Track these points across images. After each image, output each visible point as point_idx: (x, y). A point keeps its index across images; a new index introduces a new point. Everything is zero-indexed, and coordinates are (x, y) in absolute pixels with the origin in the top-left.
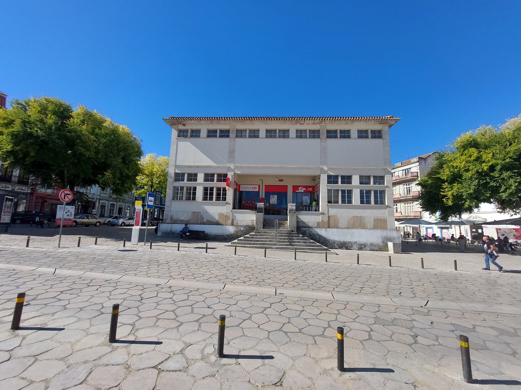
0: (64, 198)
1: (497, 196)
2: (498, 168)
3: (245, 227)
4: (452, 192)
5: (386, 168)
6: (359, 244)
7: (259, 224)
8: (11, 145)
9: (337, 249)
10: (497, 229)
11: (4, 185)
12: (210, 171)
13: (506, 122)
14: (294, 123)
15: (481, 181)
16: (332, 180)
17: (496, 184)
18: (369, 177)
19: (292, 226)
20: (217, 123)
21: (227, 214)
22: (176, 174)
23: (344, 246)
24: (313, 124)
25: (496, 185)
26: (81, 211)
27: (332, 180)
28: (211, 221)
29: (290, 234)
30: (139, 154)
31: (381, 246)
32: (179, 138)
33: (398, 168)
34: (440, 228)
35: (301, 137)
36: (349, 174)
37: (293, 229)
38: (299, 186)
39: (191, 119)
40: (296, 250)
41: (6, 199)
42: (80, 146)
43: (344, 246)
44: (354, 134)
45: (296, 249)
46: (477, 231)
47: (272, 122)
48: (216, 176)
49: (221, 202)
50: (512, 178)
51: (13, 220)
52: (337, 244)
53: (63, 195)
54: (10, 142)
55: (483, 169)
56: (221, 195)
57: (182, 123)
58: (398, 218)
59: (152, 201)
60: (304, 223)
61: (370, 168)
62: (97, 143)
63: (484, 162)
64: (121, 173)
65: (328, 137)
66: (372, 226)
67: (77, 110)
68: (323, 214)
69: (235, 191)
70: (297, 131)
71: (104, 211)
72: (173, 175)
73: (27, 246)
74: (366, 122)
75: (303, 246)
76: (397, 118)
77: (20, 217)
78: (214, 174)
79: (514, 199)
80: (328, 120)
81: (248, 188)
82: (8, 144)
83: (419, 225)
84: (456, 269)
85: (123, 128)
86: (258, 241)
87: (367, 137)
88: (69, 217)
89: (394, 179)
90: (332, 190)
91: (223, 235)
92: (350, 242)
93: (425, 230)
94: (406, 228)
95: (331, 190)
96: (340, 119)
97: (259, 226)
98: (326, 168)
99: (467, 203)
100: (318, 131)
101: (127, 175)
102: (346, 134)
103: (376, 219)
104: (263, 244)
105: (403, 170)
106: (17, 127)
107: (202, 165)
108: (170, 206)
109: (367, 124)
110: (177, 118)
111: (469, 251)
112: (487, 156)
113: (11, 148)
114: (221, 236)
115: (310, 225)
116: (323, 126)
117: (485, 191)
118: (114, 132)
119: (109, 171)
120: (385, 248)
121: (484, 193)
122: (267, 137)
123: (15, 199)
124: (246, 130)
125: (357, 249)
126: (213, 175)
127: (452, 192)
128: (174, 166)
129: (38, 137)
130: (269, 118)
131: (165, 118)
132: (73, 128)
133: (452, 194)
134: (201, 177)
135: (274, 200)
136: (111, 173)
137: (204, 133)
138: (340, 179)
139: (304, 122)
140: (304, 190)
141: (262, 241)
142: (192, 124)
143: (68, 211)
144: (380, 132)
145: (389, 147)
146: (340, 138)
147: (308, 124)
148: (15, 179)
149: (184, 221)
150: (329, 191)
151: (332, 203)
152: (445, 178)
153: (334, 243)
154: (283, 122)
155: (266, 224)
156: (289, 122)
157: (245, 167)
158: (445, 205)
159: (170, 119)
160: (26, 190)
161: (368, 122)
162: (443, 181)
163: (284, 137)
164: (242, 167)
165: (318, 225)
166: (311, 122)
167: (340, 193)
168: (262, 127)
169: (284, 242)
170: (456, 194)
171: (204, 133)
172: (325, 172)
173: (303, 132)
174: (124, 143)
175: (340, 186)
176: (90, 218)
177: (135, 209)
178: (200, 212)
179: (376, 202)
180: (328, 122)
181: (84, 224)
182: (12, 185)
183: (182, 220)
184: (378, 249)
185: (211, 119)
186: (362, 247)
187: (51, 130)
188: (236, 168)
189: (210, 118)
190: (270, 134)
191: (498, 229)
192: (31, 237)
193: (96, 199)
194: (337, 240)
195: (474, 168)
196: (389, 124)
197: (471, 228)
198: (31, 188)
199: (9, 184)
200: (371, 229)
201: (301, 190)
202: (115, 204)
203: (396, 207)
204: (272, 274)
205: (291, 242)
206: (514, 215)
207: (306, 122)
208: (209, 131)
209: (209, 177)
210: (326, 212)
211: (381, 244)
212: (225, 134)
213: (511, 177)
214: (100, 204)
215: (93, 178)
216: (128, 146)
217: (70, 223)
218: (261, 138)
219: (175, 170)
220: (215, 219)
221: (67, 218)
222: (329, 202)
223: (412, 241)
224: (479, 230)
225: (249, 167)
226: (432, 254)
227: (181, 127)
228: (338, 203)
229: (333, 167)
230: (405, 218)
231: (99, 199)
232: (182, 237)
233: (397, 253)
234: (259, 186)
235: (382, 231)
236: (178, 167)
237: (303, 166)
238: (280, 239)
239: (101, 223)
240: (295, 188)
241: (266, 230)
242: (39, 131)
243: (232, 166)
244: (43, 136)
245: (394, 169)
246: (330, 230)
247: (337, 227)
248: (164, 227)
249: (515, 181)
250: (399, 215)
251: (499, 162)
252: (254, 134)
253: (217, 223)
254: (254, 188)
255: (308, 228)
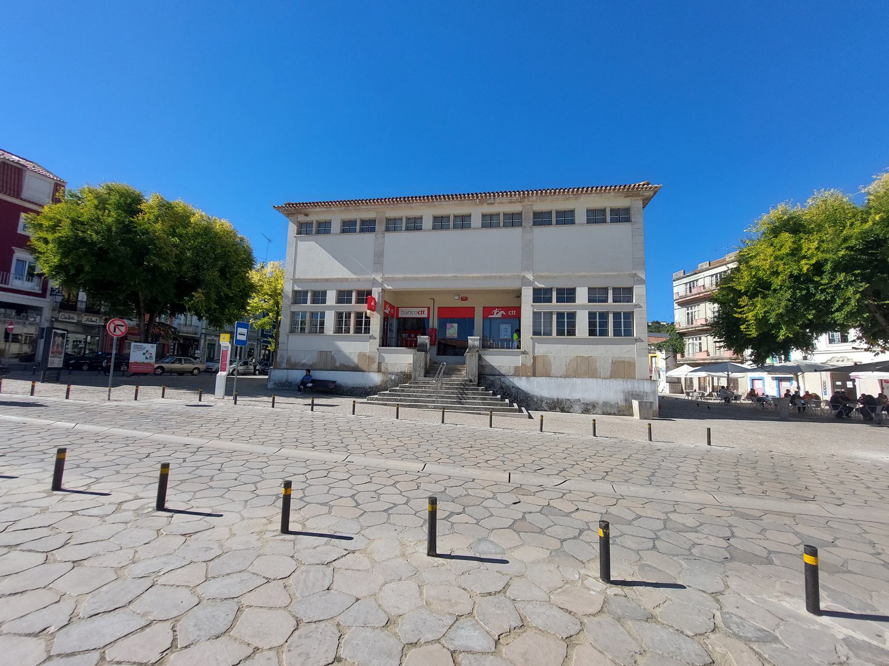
0: (115, 331)
1: (829, 318)
2: (828, 267)
3: (397, 375)
4: (754, 312)
5: (635, 274)
6: (583, 404)
7: (418, 369)
8: (59, 258)
9: (547, 411)
10: (881, 381)
11: (67, 315)
12: (345, 287)
13: (874, 180)
14: (478, 202)
15: (798, 291)
16: (541, 295)
17: (824, 297)
18: (606, 290)
19: (470, 374)
20: (355, 209)
21: (370, 354)
22: (295, 293)
23: (559, 406)
24: (509, 203)
25: (825, 299)
26: (178, 352)
27: (541, 295)
28: (346, 365)
29: (464, 388)
30: (248, 263)
31: (622, 406)
32: (300, 236)
33: (703, 272)
34: (776, 379)
35: (491, 226)
36: (570, 285)
37: (472, 378)
38: (494, 308)
39: (315, 204)
40: (491, 412)
41: (54, 334)
42: (154, 255)
43: (559, 406)
44: (581, 217)
45: (492, 410)
46: (844, 385)
47: (441, 203)
48: (354, 294)
49: (363, 335)
50: (852, 285)
51: (66, 364)
52: (546, 403)
53: (112, 327)
54: (57, 253)
55: (801, 270)
56: (363, 325)
57: (302, 211)
58: (702, 361)
59: (245, 335)
60: (492, 367)
61: (607, 273)
62: (177, 249)
63: (804, 257)
64: (218, 295)
65: (535, 224)
66: (608, 374)
67: (150, 200)
68: (524, 353)
69: (386, 319)
70: (484, 216)
71: (214, 353)
72: (290, 295)
73: (67, 397)
74: (600, 195)
75: (479, 404)
76: (656, 185)
77: (88, 362)
78: (307, 292)
79: (857, 323)
80: (535, 195)
81: (411, 313)
82: (55, 256)
83: (726, 373)
84: (709, 443)
85: (222, 223)
86: (409, 396)
87: (604, 221)
88: (148, 361)
89: (695, 293)
90: (542, 313)
91: (364, 388)
92: (569, 400)
93: (749, 383)
94: (715, 379)
95: (540, 313)
96: (555, 192)
97: (417, 374)
98: (530, 276)
99: (782, 332)
100: (520, 214)
101: (227, 296)
102: (566, 218)
103: (615, 361)
104: (415, 401)
105: (712, 276)
106: (65, 231)
107: (333, 277)
108: (286, 342)
109: (603, 197)
110: (352, 201)
111: (805, 420)
112: (810, 246)
113: (58, 262)
114: (360, 388)
115: (503, 372)
116: (528, 205)
117: (806, 310)
118: (207, 231)
119: (200, 290)
120: (626, 411)
121: (805, 313)
122: (434, 228)
123: (67, 334)
124: (401, 219)
125: (580, 411)
126: (350, 293)
127: (754, 312)
128: (292, 279)
129: (93, 244)
130: (436, 197)
131: (276, 206)
132: (143, 229)
133: (755, 316)
134: (331, 297)
135: (452, 331)
136: (203, 293)
137: (336, 227)
138: (554, 294)
139: (494, 200)
140: (503, 315)
141: (416, 396)
142: (316, 213)
143: (147, 351)
144: (627, 210)
145: (643, 237)
146: (611, 222)
147: (502, 203)
148: (81, 306)
149: (307, 365)
150: (536, 315)
151: (597, 336)
152: (742, 288)
153: (541, 401)
154: (460, 202)
155: (430, 370)
156: (469, 202)
157: (399, 279)
158: (748, 337)
159: (284, 207)
160: (98, 321)
161: (603, 194)
162: (740, 294)
163: (463, 227)
164: (393, 279)
165: (515, 372)
166: (505, 199)
167: (554, 317)
168: (427, 212)
169: (449, 398)
170: (762, 316)
171: (336, 227)
172: (527, 283)
173: (494, 218)
174: (223, 247)
175: (554, 306)
176: (183, 362)
177: (220, 345)
178: (331, 352)
179: (617, 333)
180: (534, 198)
181: (175, 372)
182: (78, 315)
183: (304, 363)
184: (616, 411)
185: (345, 204)
186: (588, 408)
187: (111, 233)
188: (385, 280)
189: (400, 198)
190: (440, 223)
191: (883, 381)
192: (72, 387)
193: (199, 334)
194: (546, 396)
195: (787, 269)
196: (643, 196)
197: (834, 379)
198: (104, 318)
199: (74, 313)
200: (605, 378)
201: (497, 314)
202: (254, 345)
203: (700, 341)
204: (518, 461)
205: (462, 398)
206: (880, 353)
207: (497, 200)
208: (436, 218)
209: (343, 297)
210: (530, 350)
211: (622, 403)
212: (368, 226)
213: (850, 283)
214: (207, 342)
215: (177, 302)
216: (229, 251)
217: (150, 369)
218: (425, 230)
219: (293, 286)
220: (353, 362)
221: (146, 362)
222: (536, 333)
223: (716, 401)
224: (848, 383)
225: (405, 279)
226: (730, 422)
227: (302, 218)
228: (551, 335)
229: (543, 274)
230: (713, 361)
231: (205, 334)
232: (300, 390)
233: (645, 419)
234: (429, 308)
235: (625, 381)
236: (297, 281)
237: (492, 275)
238: (446, 393)
239: (201, 370)
240: (488, 311)
241: (427, 379)
242: (94, 236)
243: (378, 277)
244: (100, 243)
245: (696, 274)
246: (535, 380)
247: (548, 375)
248: (278, 374)
249: (857, 290)
250: (703, 355)
251: (828, 256)
252: (414, 224)
253: (356, 369)
254: (420, 313)
255: (498, 377)
